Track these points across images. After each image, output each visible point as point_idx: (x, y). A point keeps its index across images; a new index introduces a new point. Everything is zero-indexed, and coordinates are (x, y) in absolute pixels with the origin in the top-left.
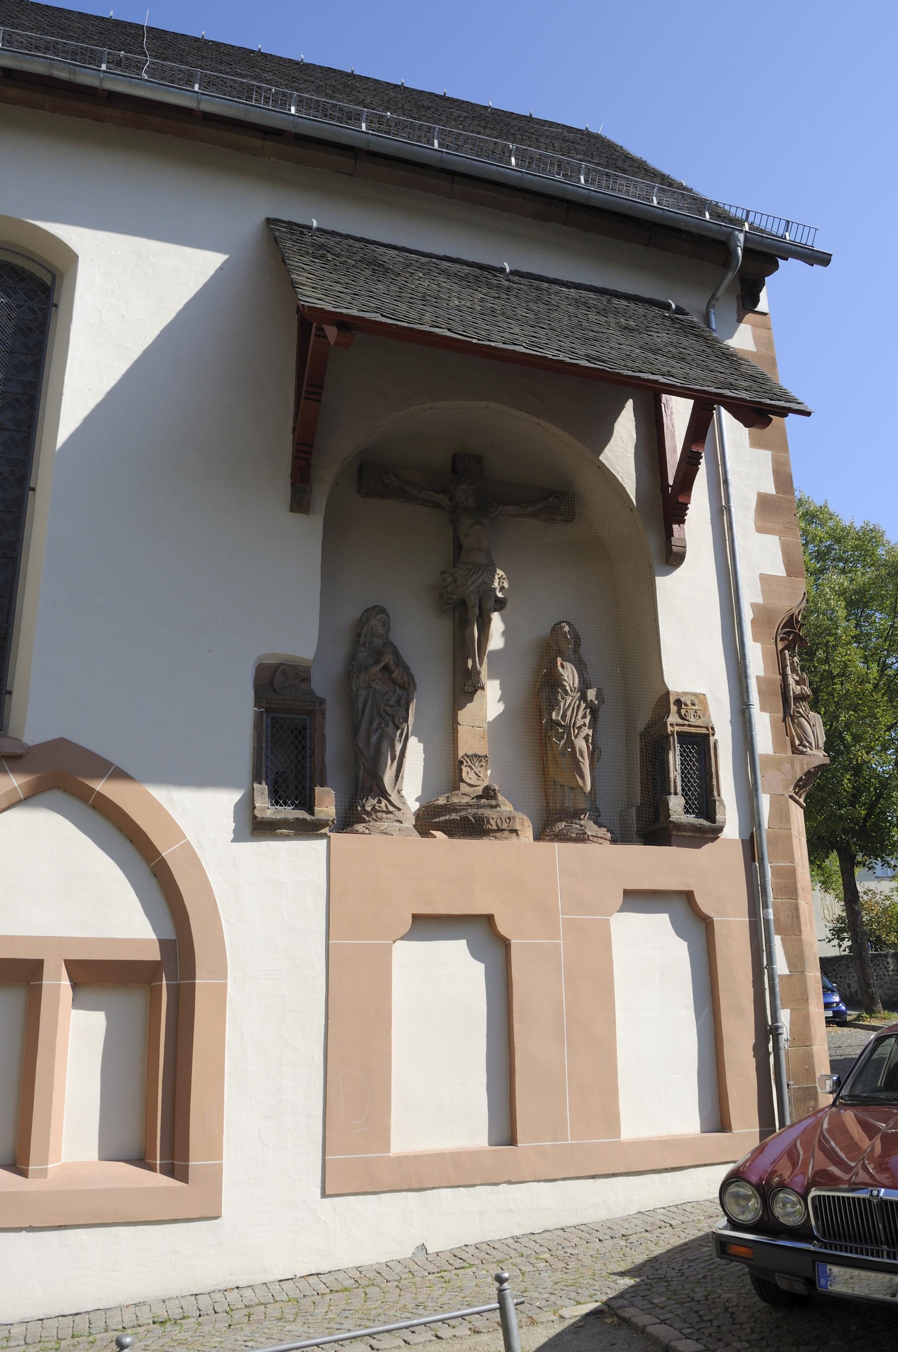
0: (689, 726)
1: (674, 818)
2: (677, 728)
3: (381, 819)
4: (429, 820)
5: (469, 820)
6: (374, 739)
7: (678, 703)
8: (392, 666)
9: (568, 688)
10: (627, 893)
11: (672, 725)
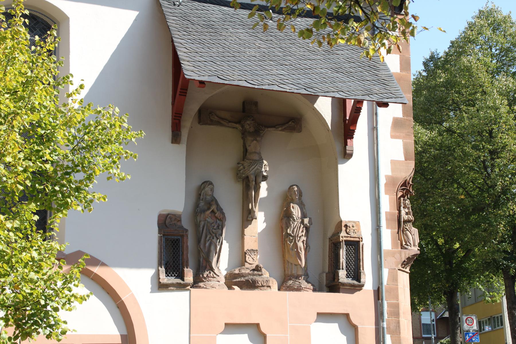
0: (351, 237)
1: (341, 280)
2: (345, 239)
3: (210, 281)
4: (232, 281)
5: (249, 282)
6: (207, 244)
7: (346, 226)
8: (216, 210)
9: (295, 218)
10: (318, 314)
11: (342, 237)
